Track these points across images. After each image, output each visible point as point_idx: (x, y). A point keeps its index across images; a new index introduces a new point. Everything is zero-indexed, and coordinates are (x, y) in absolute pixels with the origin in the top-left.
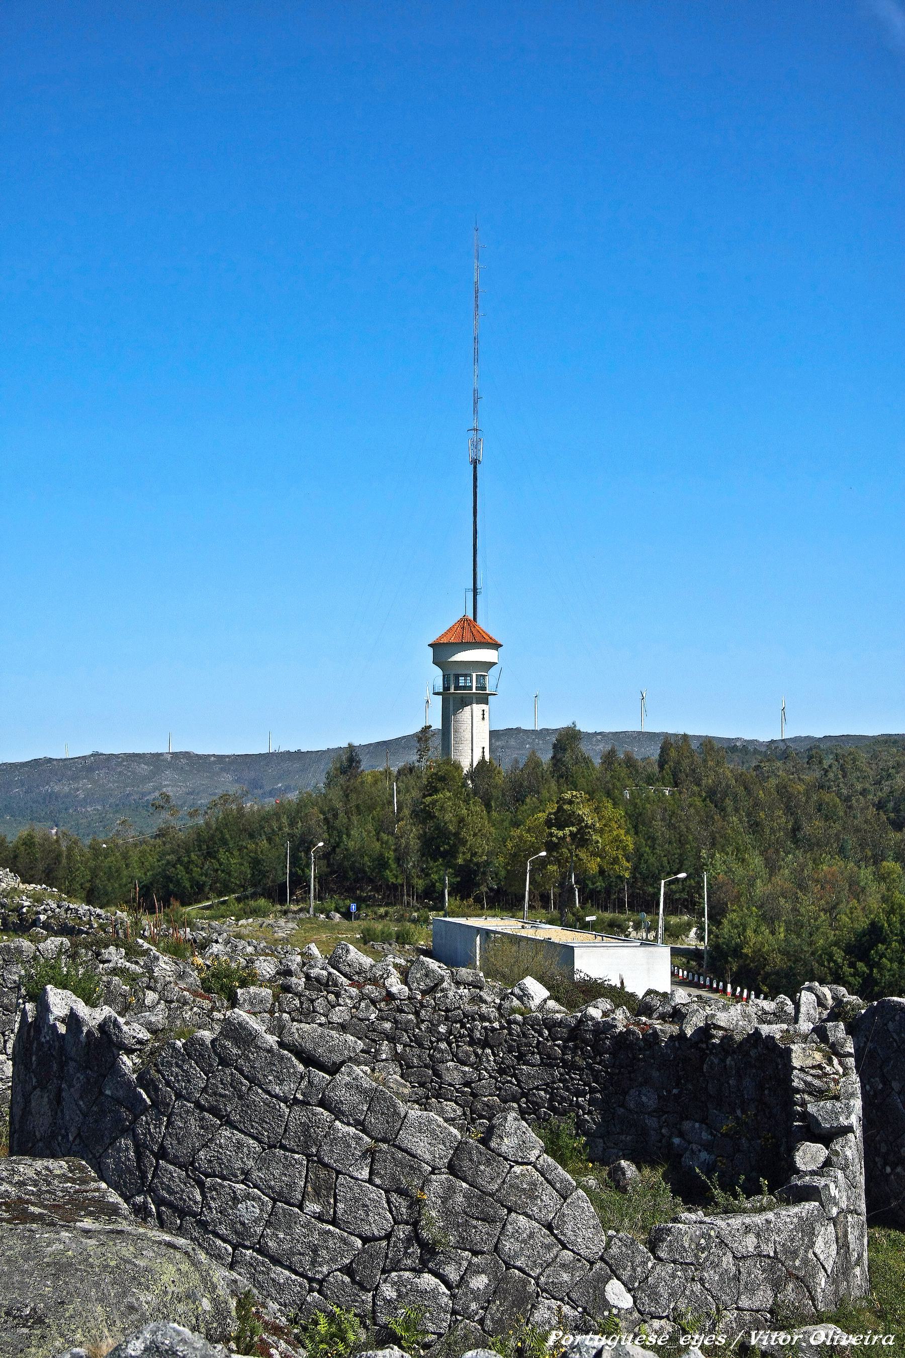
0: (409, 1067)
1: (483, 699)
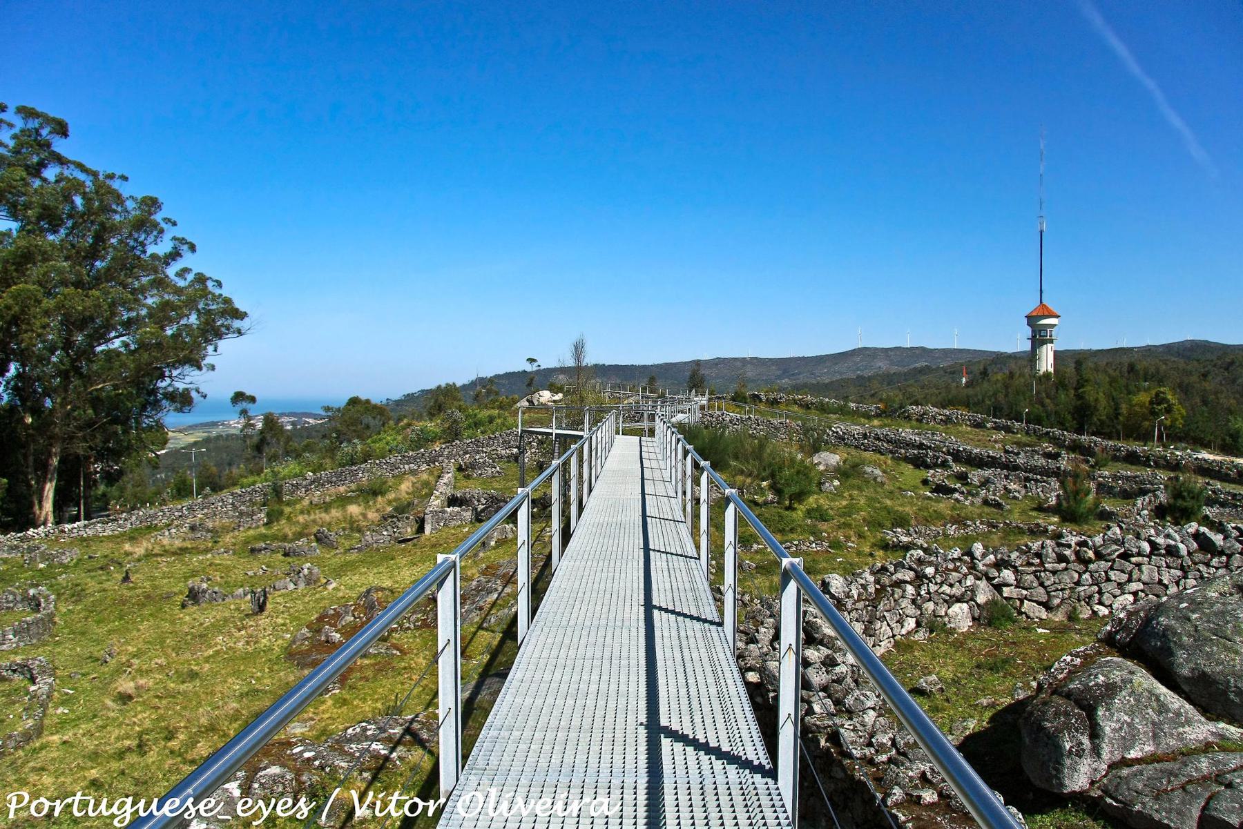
1: (1051, 341)
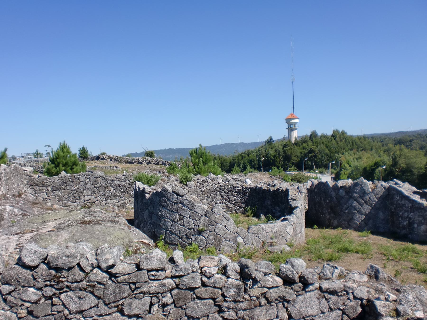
0: (223, 197)
1: (296, 129)
